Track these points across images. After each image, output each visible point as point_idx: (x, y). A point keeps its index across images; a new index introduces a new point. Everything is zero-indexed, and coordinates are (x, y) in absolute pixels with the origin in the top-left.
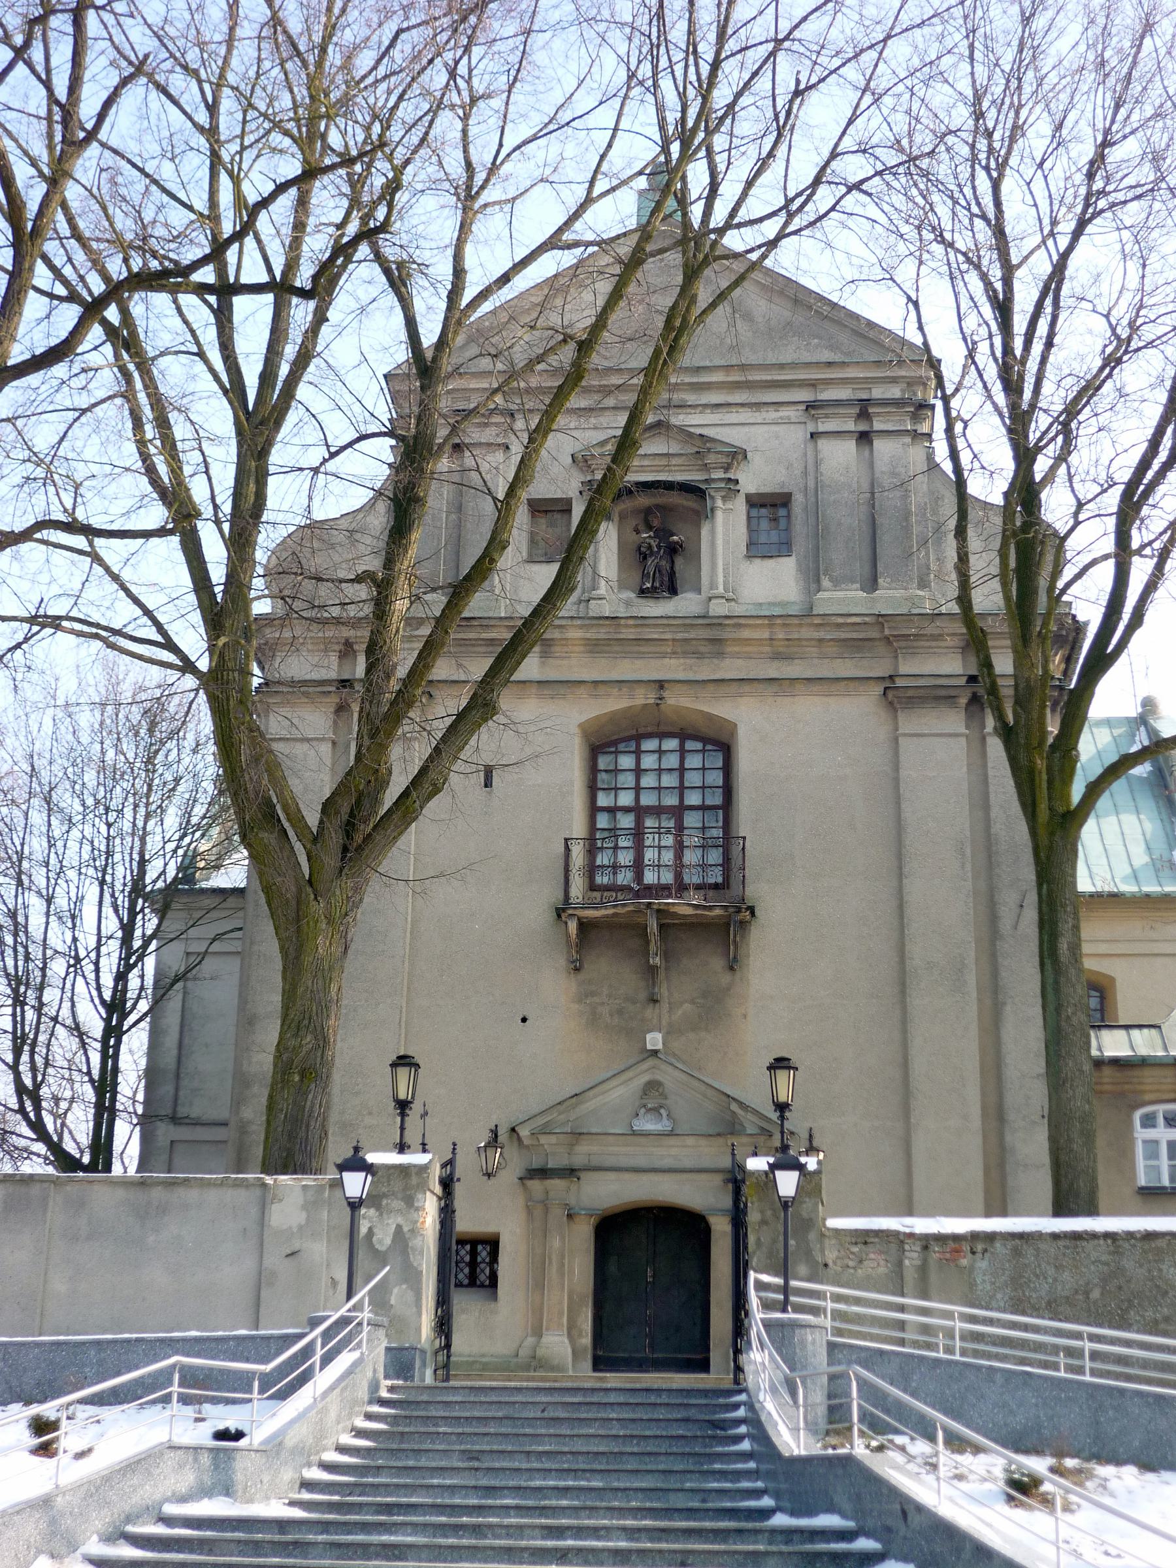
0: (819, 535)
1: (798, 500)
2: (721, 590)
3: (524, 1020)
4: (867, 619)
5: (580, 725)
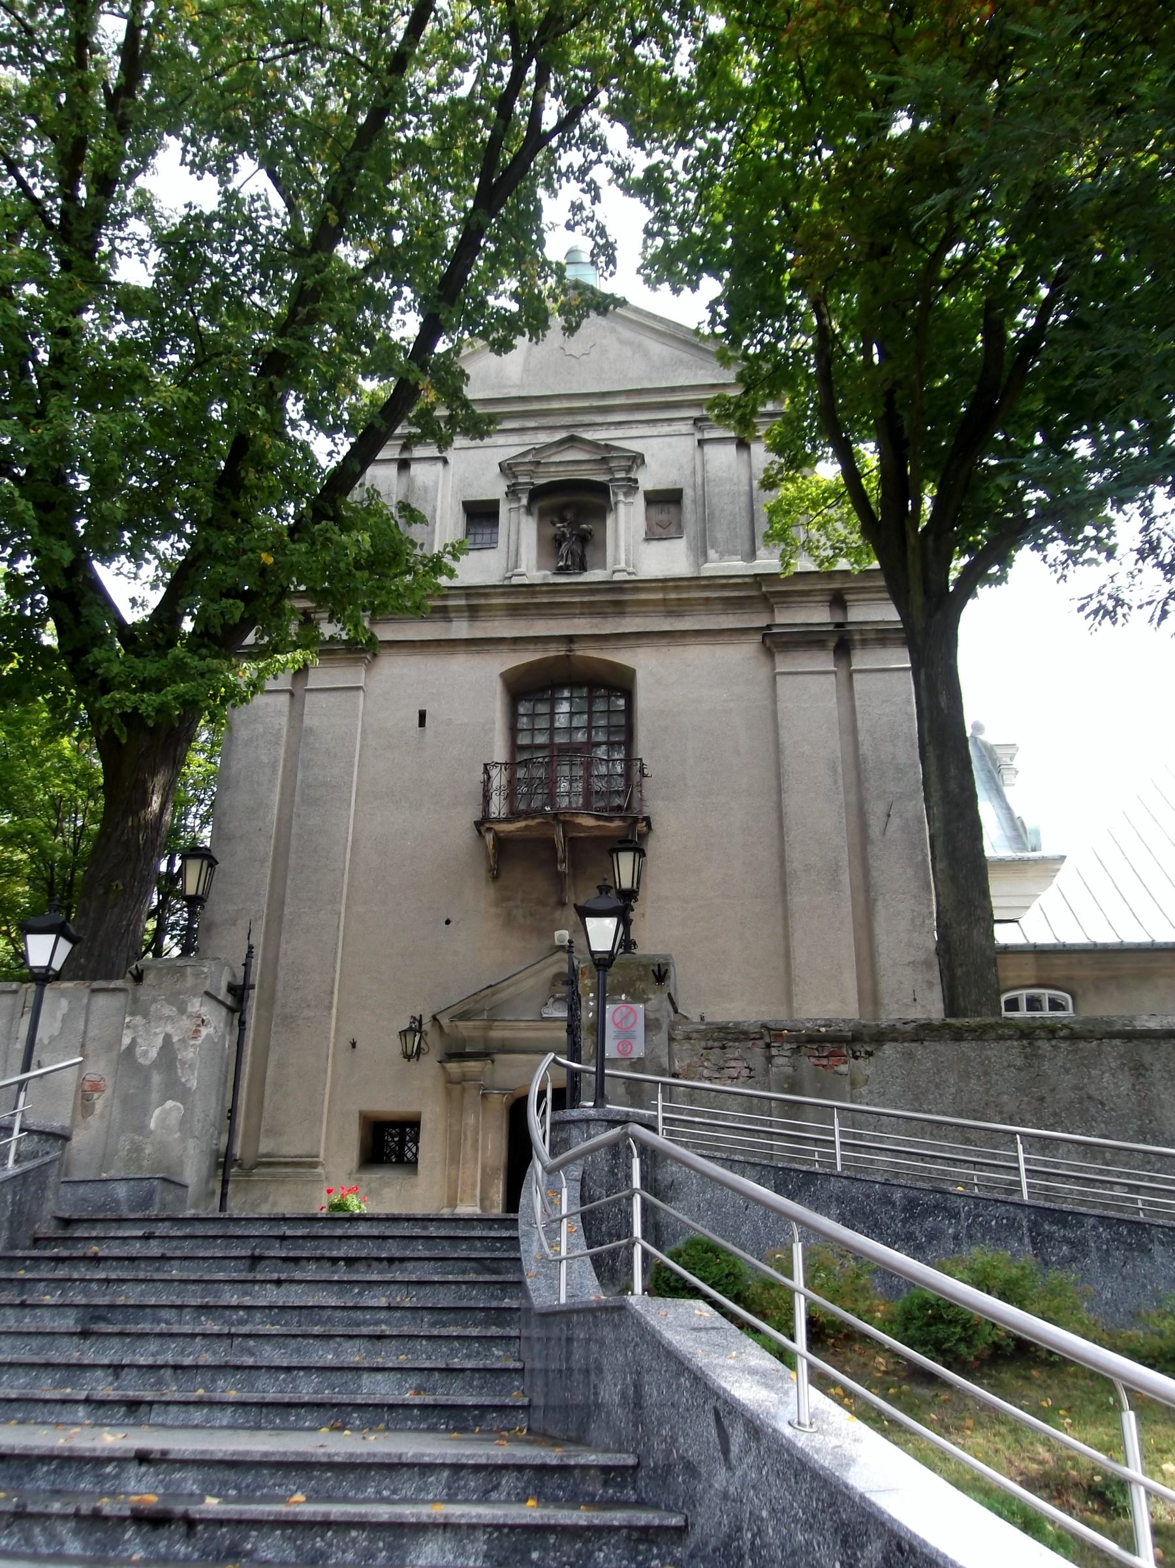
0: (706, 521)
2: (623, 565)
3: (448, 922)
5: (503, 675)
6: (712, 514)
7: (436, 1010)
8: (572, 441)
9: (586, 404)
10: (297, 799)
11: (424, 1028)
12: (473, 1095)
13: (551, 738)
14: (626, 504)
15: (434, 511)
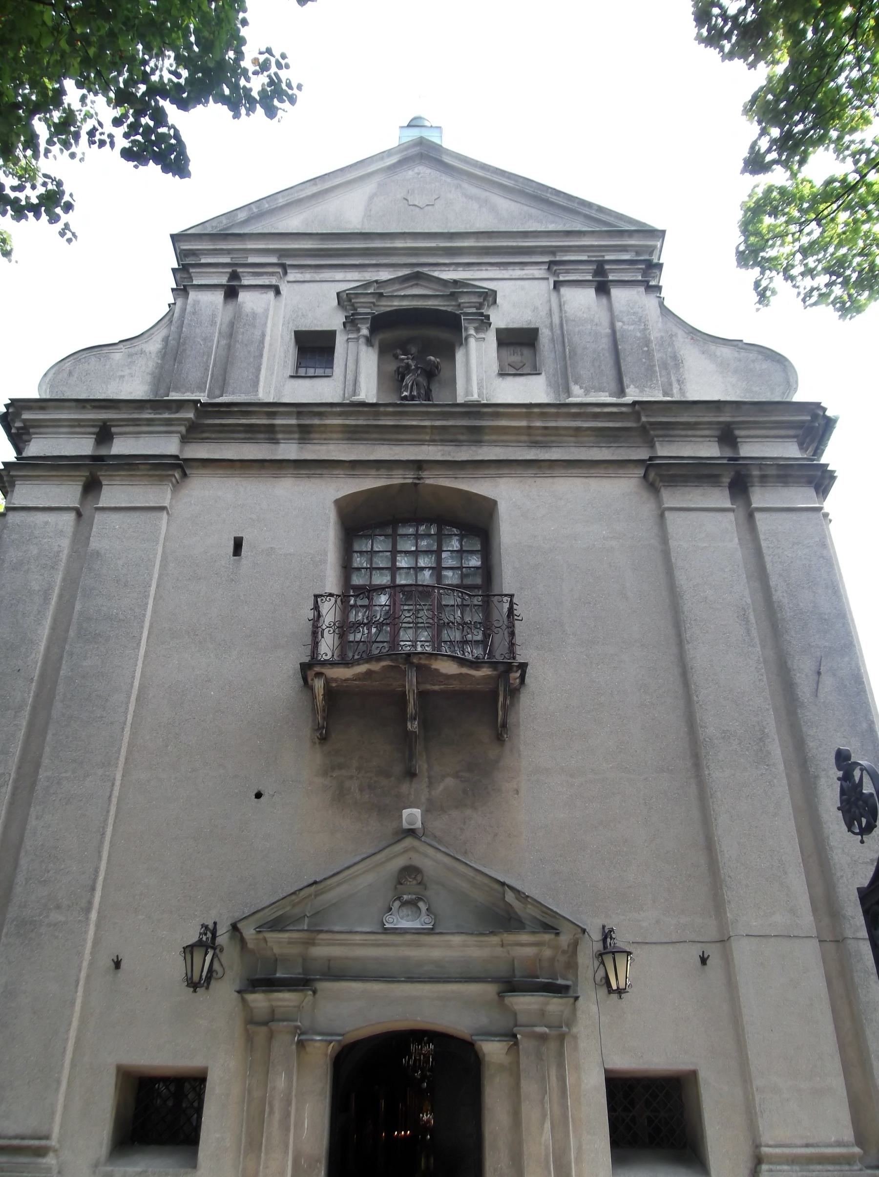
1: (545, 337)
3: (259, 795)
4: (624, 409)
5: (338, 503)
6: (573, 351)
7: (238, 915)
8: (417, 278)
9: (433, 245)
10: (72, 633)
11: (220, 940)
12: (284, 1044)
13: (393, 578)
14: (477, 339)
15: (263, 335)
